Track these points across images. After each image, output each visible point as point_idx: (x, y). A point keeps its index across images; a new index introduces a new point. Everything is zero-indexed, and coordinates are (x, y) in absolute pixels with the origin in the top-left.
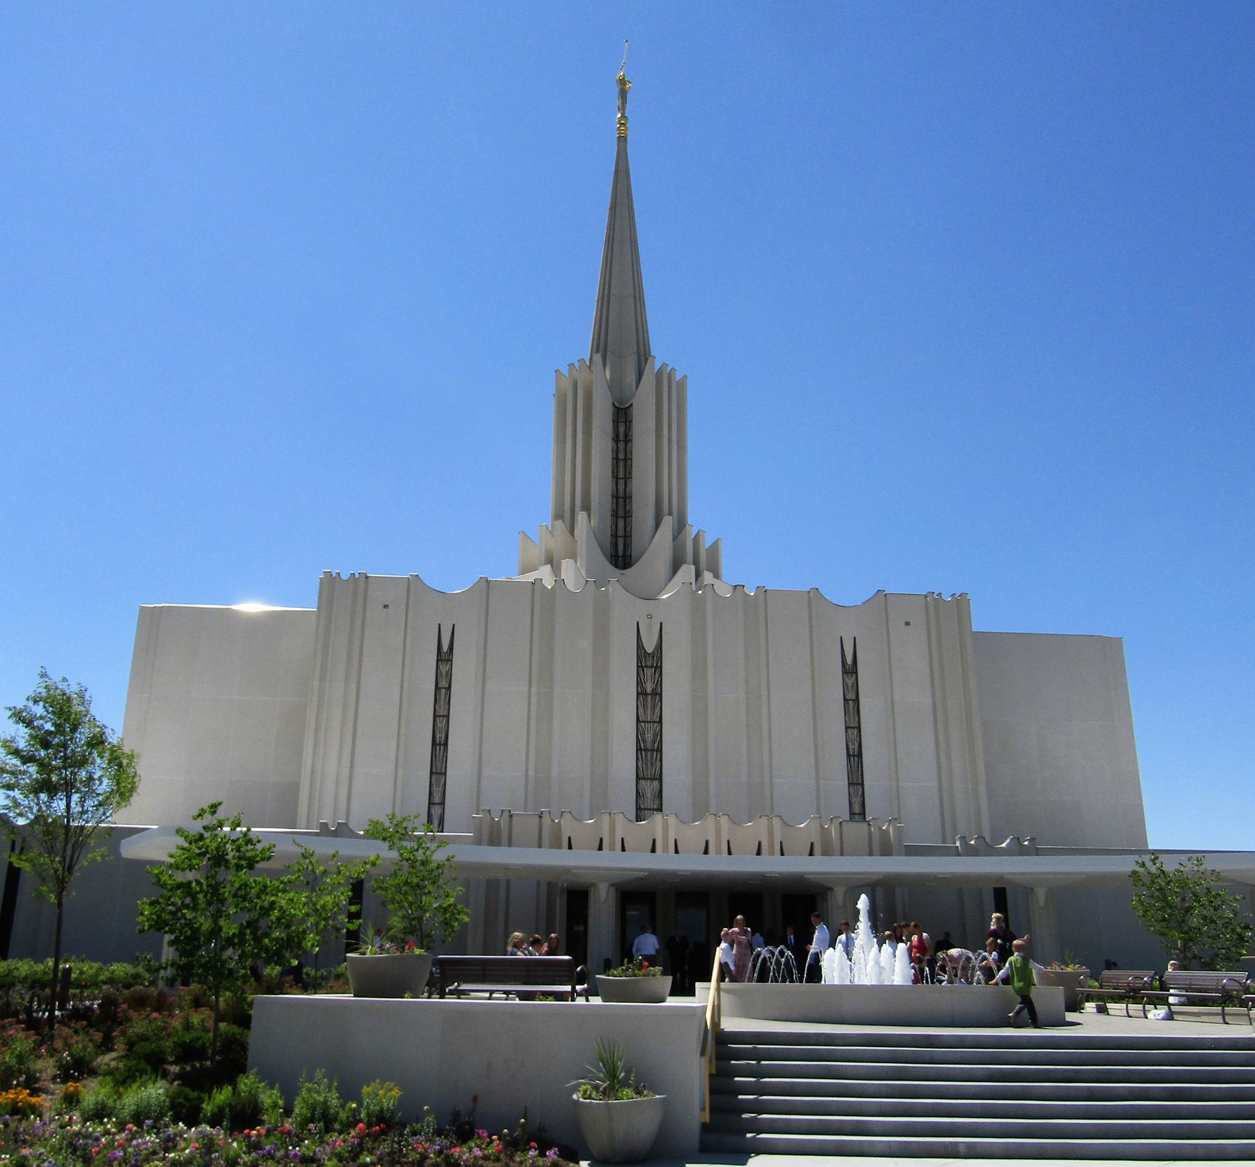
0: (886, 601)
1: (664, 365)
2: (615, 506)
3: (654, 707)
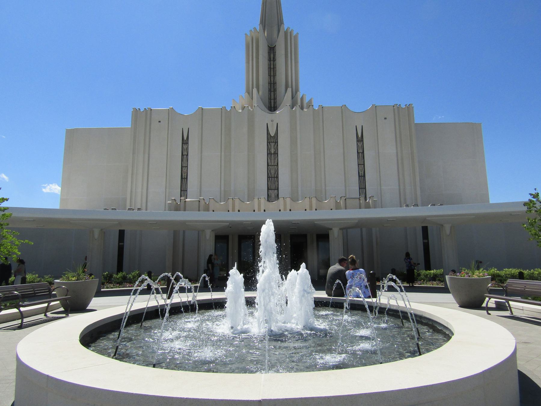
0: (376, 108)
1: (288, 28)
2: (270, 87)
3: (275, 159)
